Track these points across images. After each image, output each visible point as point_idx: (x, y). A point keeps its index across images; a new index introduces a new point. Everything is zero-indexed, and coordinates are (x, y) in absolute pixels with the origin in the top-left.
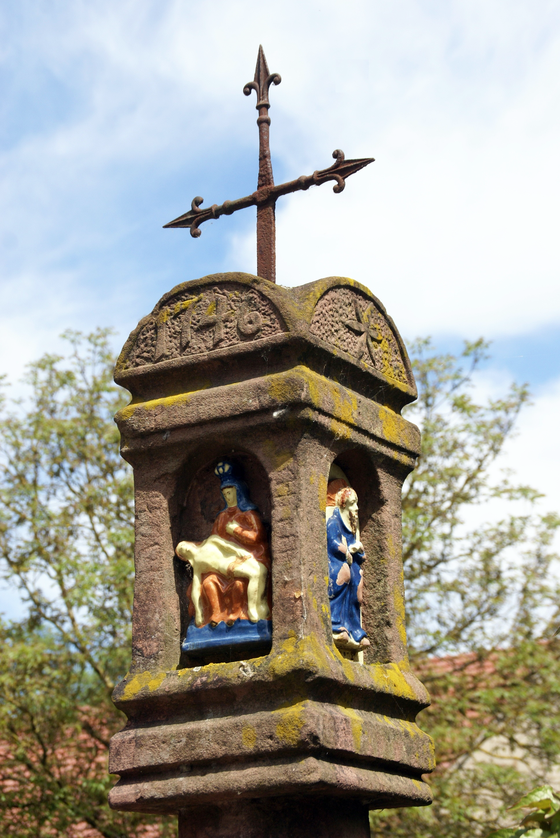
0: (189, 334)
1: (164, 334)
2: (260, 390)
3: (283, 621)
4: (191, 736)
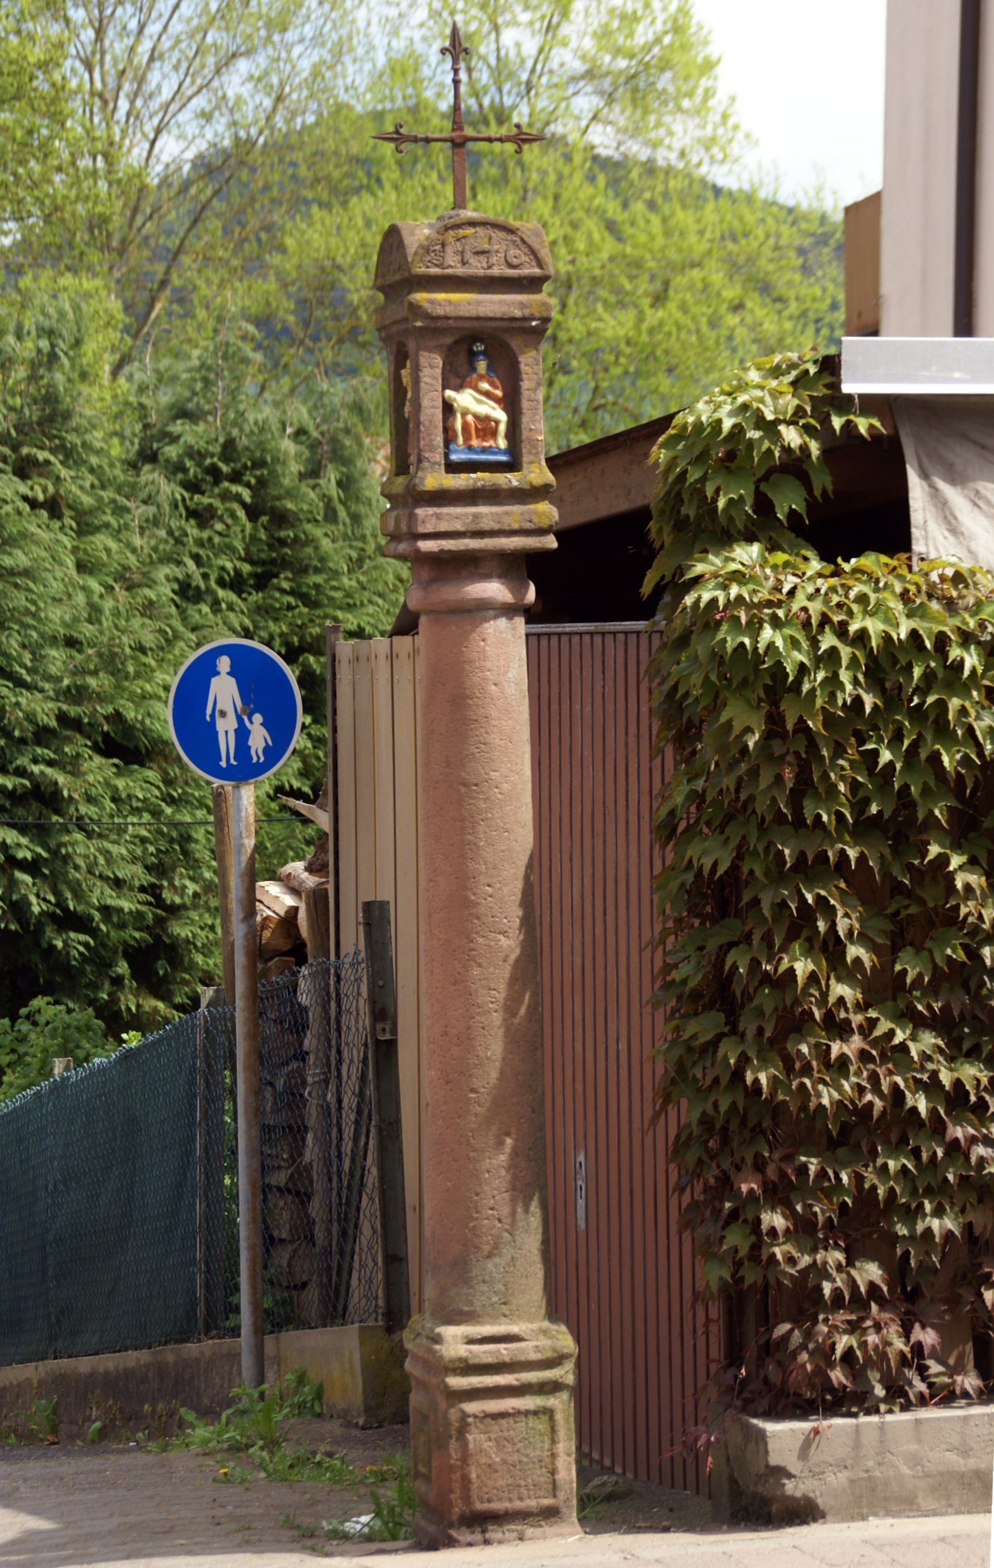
0: (468, 256)
1: (449, 250)
2: (522, 305)
3: (530, 453)
4: (476, 516)
